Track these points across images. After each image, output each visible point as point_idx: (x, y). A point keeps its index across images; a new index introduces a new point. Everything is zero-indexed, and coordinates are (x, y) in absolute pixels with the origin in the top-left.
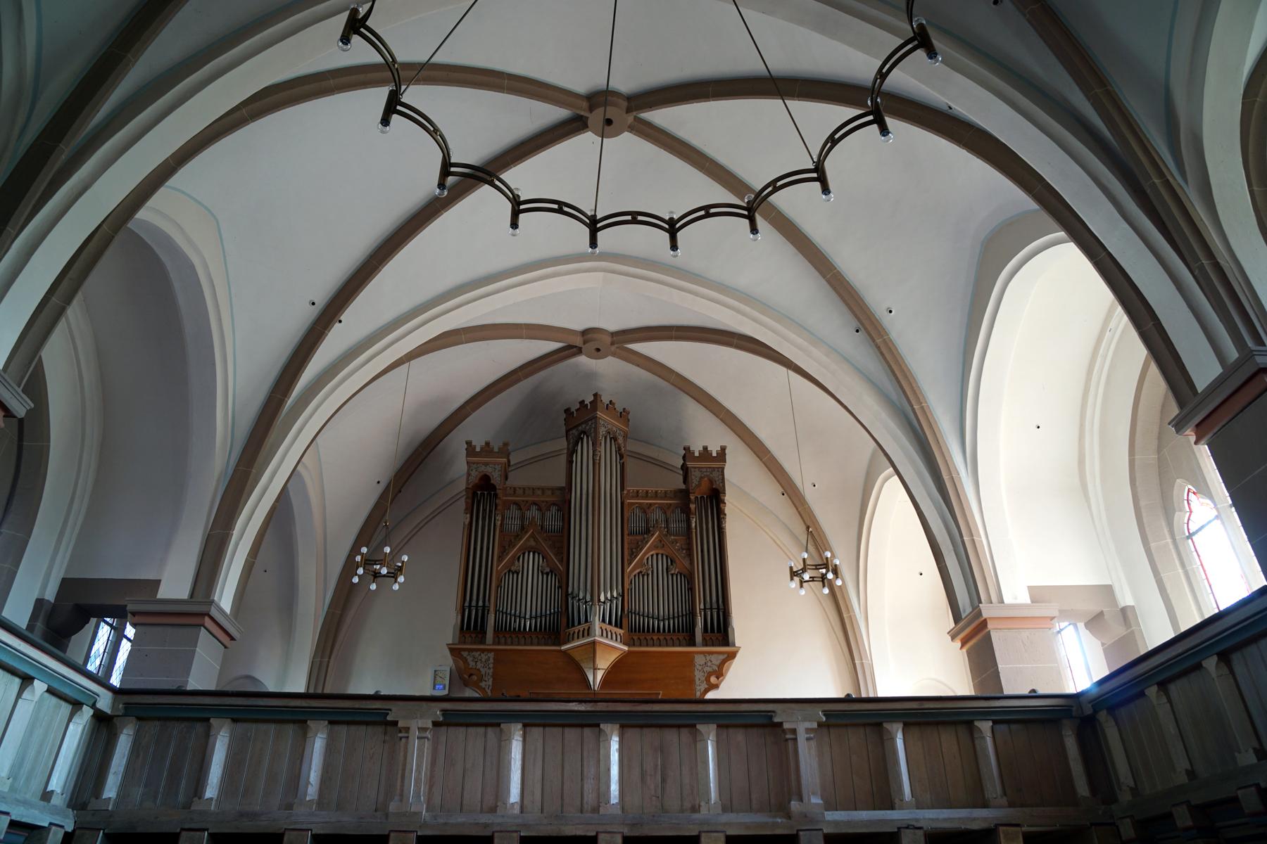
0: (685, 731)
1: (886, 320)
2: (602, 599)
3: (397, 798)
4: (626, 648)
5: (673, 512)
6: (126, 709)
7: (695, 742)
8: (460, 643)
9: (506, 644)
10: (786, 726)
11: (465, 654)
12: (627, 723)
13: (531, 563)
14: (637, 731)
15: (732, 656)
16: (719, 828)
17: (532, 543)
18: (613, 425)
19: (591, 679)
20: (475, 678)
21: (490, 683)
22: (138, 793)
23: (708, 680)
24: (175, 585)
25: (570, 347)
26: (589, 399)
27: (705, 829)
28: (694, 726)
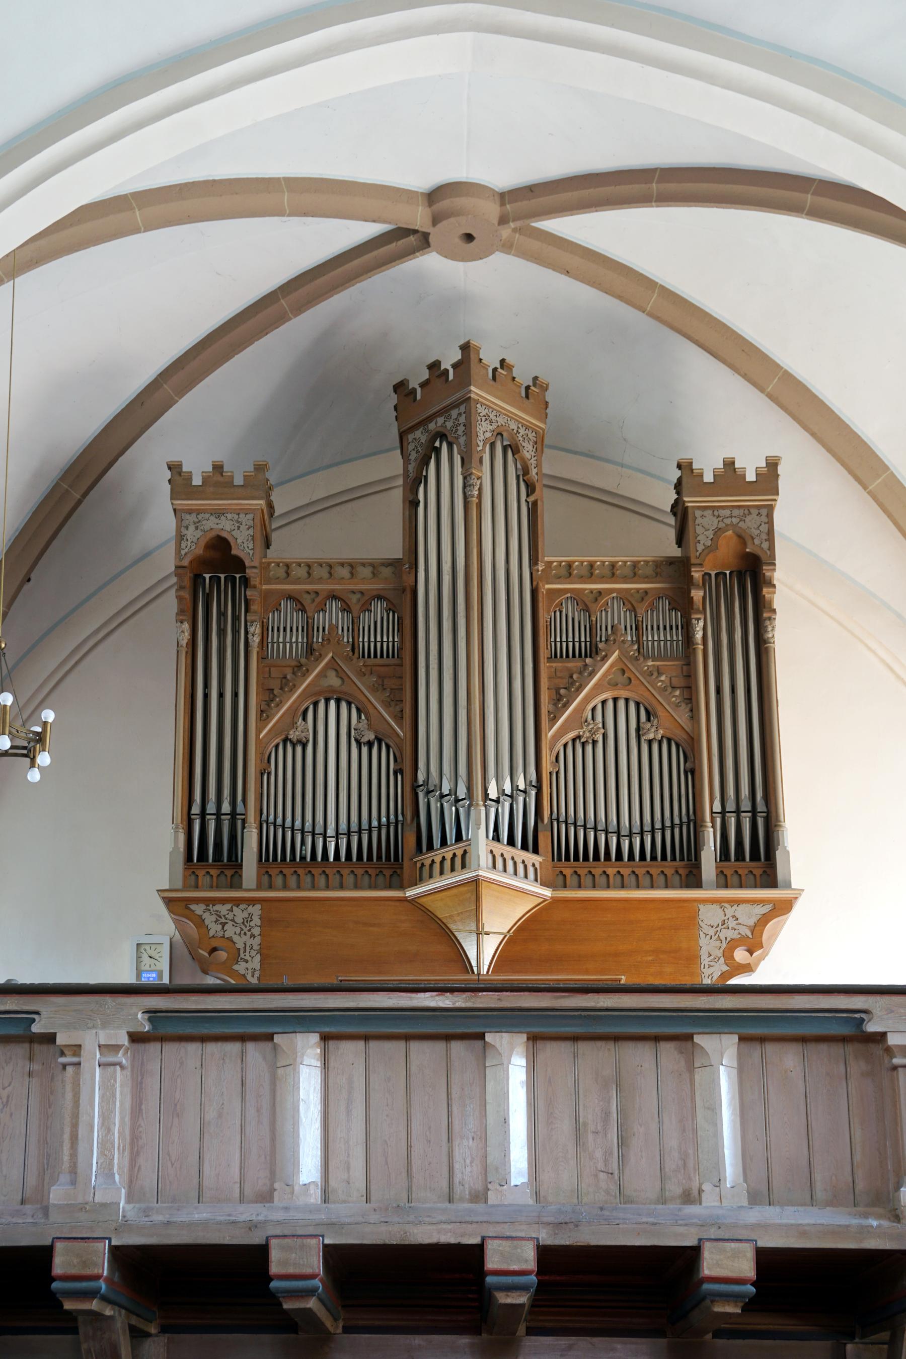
0: (667, 1048)
2: (493, 793)
3: (64, 1178)
4: (547, 893)
5: (652, 608)
7: (691, 1068)
8: (185, 888)
9: (285, 887)
10: (893, 1040)
11: (198, 909)
12: (541, 1030)
14: (565, 1048)
15: (783, 907)
16: (744, 1234)
17: (333, 681)
19: (472, 954)
20: (223, 955)
21: (256, 963)
25: (401, 232)
26: (450, 358)
27: (713, 1233)
28: (689, 1037)
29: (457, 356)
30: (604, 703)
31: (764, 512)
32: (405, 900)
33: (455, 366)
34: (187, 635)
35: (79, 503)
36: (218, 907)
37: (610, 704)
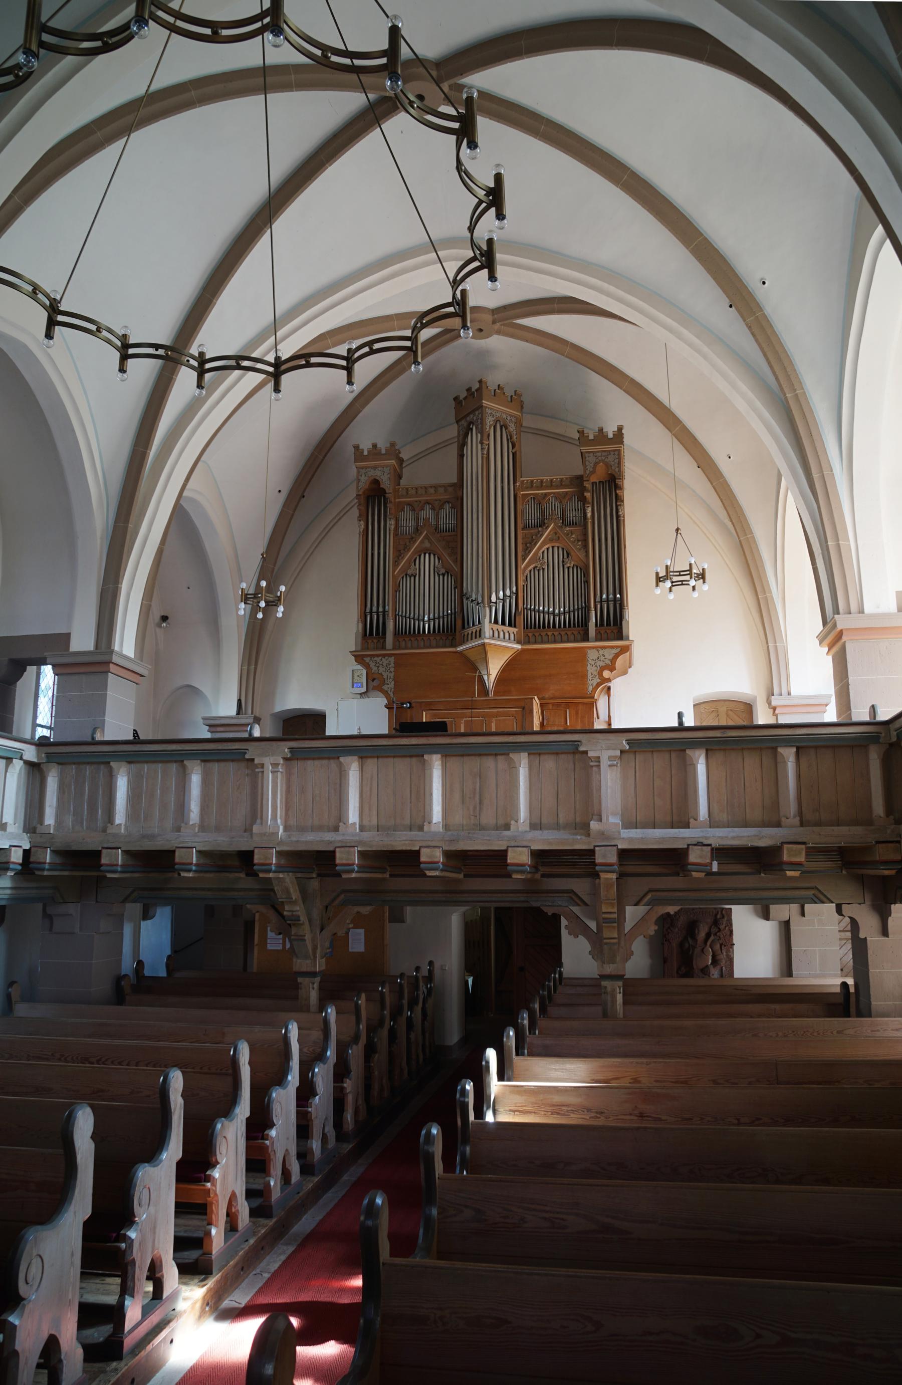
1: (760, 293)
2: (494, 599)
3: (258, 821)
4: (519, 647)
6: (47, 757)
8: (363, 649)
10: (591, 754)
11: (367, 660)
13: (427, 563)
16: (525, 844)
18: (503, 412)
21: (392, 685)
22: (69, 820)
23: (600, 674)
24: (83, 641)
27: (513, 844)
29: (477, 386)
30: (548, 549)
31: (616, 453)
32: (457, 652)
33: (477, 390)
34: (363, 527)
35: (322, 460)
36: (376, 658)
37: (551, 550)
